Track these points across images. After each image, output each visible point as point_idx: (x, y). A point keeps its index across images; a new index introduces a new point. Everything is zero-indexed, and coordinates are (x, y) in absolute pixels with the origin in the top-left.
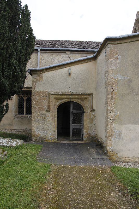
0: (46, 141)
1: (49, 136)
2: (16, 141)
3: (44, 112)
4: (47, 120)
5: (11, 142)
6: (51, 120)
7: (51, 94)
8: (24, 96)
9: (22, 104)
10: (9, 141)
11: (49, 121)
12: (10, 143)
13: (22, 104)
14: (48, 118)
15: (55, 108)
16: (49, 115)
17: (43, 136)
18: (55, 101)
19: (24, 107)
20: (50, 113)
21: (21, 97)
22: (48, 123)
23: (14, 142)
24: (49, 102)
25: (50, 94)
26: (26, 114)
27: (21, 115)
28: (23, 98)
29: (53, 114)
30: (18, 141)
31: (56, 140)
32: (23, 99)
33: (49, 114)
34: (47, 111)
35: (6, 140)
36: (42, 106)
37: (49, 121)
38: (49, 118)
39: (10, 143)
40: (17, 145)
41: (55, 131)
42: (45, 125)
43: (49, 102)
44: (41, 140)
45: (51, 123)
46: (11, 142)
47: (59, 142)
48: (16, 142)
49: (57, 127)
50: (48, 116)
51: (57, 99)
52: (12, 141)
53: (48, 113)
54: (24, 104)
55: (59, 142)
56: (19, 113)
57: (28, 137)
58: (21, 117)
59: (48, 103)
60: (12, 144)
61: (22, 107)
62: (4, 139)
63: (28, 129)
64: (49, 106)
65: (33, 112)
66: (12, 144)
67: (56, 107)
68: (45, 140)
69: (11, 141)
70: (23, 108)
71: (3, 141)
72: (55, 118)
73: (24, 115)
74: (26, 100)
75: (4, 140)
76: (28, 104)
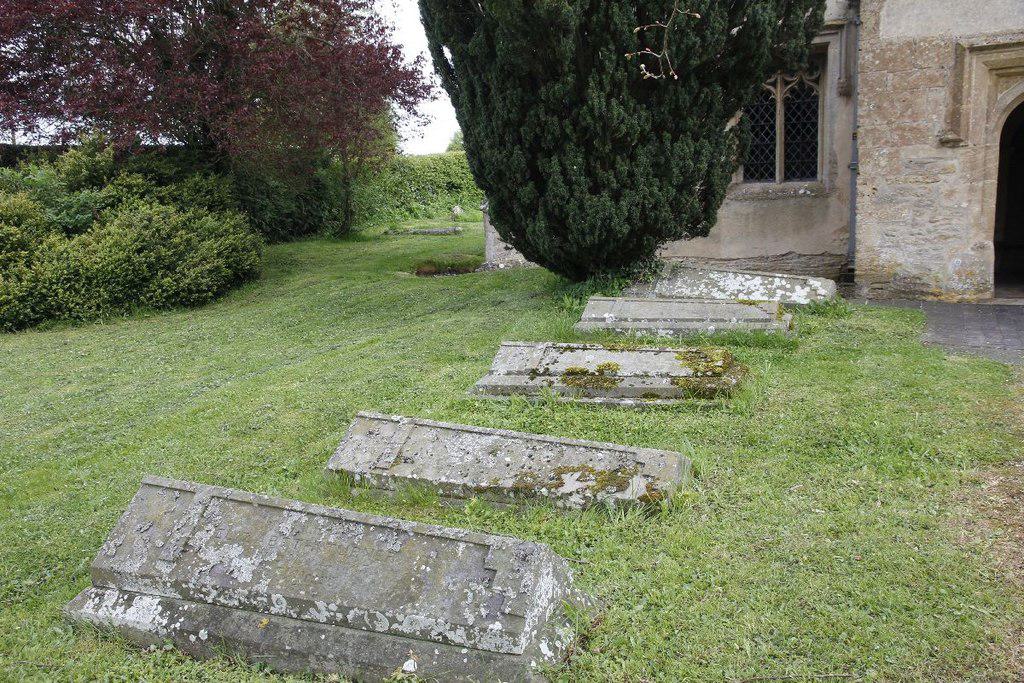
0: (930, 298)
1: (950, 269)
2: (805, 284)
3: (926, 151)
4: (944, 188)
5: (782, 288)
6: (963, 186)
7: (973, 49)
8: (774, 84)
9: (763, 128)
10: (772, 283)
11: (951, 193)
12: (780, 292)
13: (763, 128)
14: (946, 183)
15: (992, 125)
16: (955, 162)
17: (915, 272)
18: (989, 83)
19: (773, 139)
20: (961, 151)
21: (801, 83)
22: (945, 203)
23: (798, 288)
24: (957, 96)
25: (961, 52)
26: (787, 177)
27: (757, 187)
28: (769, 93)
29: (980, 156)
30: (815, 283)
31: (988, 295)
32: (766, 98)
33: (955, 159)
34: (943, 143)
35: (758, 280)
36: (914, 117)
37: (951, 193)
38: (952, 178)
39: (780, 292)
40: (812, 301)
41: (982, 247)
42: (926, 218)
43: (957, 96)
44: (904, 292)
45: (965, 205)
46: (782, 288)
47: (1000, 301)
48: (807, 289)
49: (996, 232)
50: (946, 171)
51: (1002, 73)
52: (788, 286)
53: (949, 152)
54: (773, 127)
55: (1000, 301)
56: (745, 176)
57: (130, 606)
58: (764, 197)
59: (950, 100)
60: (788, 294)
61: (763, 140)
62: (747, 276)
63: (800, 256)
64: (955, 118)
65: (864, 155)
66: (788, 294)
67: (998, 121)
68: (928, 293)
69: (784, 282)
70: (767, 146)
71: (748, 283)
72: (986, 177)
73: (773, 186)
74: (787, 102)
75: (751, 282)
76: (794, 126)
